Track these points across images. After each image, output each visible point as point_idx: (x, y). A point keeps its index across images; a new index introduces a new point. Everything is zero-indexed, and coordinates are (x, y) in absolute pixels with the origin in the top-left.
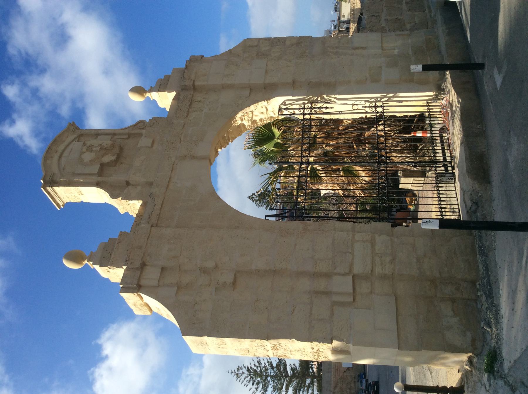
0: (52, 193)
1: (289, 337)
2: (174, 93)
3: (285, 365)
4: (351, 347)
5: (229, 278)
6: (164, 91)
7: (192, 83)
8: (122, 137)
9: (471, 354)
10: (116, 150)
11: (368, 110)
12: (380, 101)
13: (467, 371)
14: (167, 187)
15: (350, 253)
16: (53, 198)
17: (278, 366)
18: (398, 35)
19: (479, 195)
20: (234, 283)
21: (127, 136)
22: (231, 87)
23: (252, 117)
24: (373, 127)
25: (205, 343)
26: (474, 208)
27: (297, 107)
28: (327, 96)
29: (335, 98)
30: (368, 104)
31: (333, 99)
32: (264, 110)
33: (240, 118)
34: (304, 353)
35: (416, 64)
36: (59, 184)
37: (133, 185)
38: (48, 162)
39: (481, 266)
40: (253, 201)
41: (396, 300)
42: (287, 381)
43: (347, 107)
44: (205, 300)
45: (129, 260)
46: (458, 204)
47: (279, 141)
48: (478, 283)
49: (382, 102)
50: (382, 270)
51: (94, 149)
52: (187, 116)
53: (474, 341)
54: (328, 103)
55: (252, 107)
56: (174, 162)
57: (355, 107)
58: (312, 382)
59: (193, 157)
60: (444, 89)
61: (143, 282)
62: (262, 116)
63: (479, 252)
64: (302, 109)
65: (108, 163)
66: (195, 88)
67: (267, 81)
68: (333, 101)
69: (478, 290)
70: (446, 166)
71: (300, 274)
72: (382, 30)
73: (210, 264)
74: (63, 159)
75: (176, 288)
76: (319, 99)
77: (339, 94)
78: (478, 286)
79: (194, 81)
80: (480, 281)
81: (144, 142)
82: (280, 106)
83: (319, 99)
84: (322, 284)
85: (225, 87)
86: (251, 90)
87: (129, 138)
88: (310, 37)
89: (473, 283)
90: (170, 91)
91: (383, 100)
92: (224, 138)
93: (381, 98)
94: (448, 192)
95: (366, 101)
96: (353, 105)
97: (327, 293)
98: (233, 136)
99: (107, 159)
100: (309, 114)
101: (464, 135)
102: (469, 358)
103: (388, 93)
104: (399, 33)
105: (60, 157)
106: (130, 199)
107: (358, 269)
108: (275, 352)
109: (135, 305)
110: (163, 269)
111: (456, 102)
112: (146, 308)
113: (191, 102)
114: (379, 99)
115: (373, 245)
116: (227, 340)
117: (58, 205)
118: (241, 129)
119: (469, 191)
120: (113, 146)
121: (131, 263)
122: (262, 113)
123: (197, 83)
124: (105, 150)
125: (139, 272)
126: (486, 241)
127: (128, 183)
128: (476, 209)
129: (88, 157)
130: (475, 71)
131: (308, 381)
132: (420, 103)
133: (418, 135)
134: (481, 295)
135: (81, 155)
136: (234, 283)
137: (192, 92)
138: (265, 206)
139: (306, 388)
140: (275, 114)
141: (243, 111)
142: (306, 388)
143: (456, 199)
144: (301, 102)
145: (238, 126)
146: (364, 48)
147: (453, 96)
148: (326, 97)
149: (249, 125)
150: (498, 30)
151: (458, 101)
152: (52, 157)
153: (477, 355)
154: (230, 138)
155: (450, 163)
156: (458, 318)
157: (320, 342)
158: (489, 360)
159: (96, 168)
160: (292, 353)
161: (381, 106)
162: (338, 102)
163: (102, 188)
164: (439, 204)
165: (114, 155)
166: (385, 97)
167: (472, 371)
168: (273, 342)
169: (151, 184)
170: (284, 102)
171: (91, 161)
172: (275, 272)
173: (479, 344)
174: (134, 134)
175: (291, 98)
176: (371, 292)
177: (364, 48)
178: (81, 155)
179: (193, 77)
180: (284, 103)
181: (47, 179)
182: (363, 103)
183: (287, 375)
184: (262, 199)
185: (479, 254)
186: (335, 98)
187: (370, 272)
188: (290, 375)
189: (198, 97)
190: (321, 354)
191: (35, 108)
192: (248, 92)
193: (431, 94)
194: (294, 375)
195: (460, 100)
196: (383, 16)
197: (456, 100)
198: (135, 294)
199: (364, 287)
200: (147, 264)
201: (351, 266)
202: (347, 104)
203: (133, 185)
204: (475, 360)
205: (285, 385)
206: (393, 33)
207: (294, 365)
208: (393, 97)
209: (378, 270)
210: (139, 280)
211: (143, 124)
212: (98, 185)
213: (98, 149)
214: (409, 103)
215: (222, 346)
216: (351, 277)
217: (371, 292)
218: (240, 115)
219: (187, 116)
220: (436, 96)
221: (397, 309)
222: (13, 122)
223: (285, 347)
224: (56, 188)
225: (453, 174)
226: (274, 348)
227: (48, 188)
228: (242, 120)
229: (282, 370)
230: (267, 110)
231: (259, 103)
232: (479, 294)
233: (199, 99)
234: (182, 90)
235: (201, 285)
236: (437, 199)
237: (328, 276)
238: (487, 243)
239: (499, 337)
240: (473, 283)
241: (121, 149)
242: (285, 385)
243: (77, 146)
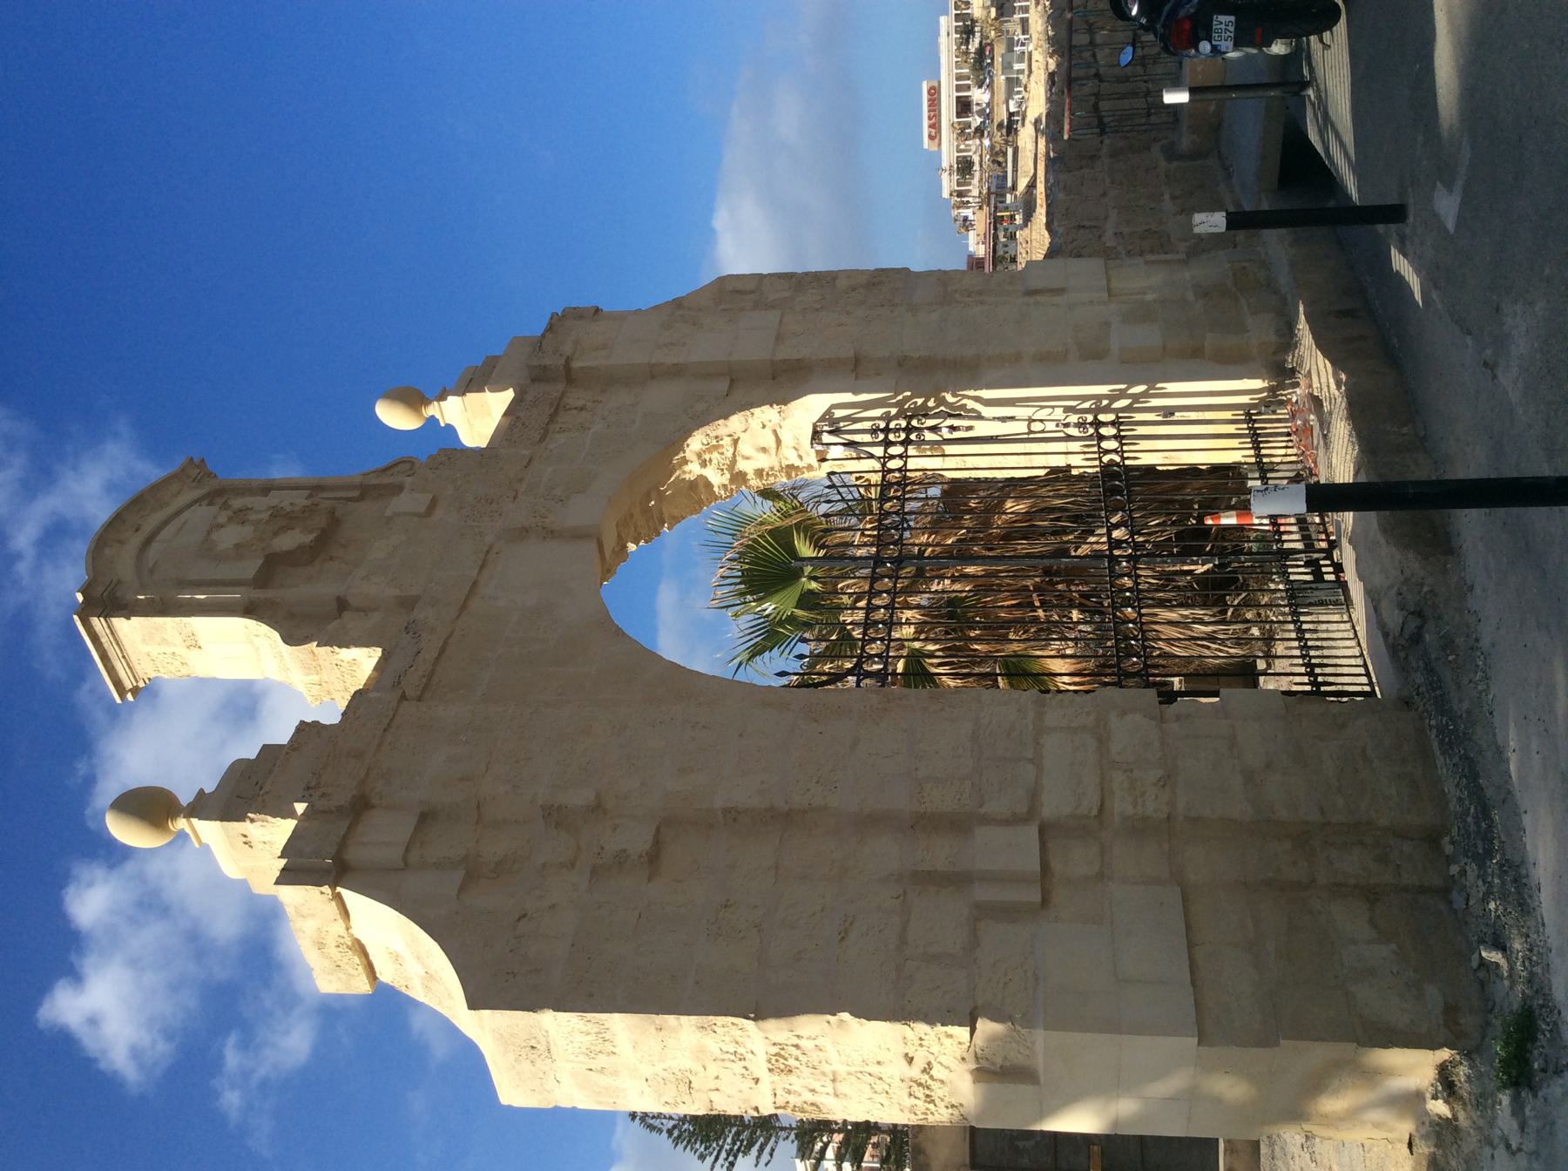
0: (104, 640)
1: (828, 1007)
2: (509, 395)
4: (1041, 1044)
5: (637, 840)
6: (481, 390)
7: (562, 361)
8: (343, 494)
9: (1445, 1054)
10: (321, 521)
11: (1074, 431)
12: (1107, 410)
13: (1442, 1131)
14: (464, 607)
15: (1031, 761)
16: (104, 657)
18: (1153, 262)
19: (1425, 589)
20: (653, 858)
21: (356, 494)
22: (677, 371)
23: (734, 461)
24: (1092, 533)
25: (541, 1047)
26: (1413, 625)
27: (867, 425)
28: (954, 395)
29: (977, 399)
30: (1074, 418)
31: (971, 404)
32: (770, 442)
33: (699, 455)
34: (879, 1086)
35: (1212, 208)
36: (128, 610)
37: (358, 610)
38: (108, 552)
39: (1450, 788)
41: (1185, 899)
43: (1016, 433)
44: (553, 907)
45: (318, 786)
46: (1362, 655)
47: (814, 585)
48: (1447, 839)
49: (1117, 411)
50: (1135, 805)
51: (253, 517)
52: (542, 439)
53: (1451, 1010)
54: (959, 416)
55: (736, 422)
56: (491, 547)
57: (1036, 426)
59: (551, 534)
60: (1293, 371)
61: (353, 854)
62: (764, 462)
63: (1441, 743)
64: (882, 431)
65: (289, 553)
66: (569, 376)
67: (780, 356)
68: (973, 410)
69: (1450, 860)
70: (1314, 565)
71: (868, 823)
72: (1108, 254)
74: (155, 546)
75: (458, 875)
76: (931, 403)
77: (989, 386)
78: (1448, 849)
79: (568, 360)
80: (1454, 831)
81: (406, 502)
82: (815, 426)
83: (931, 403)
84: (940, 853)
85: (653, 374)
86: (732, 380)
87: (361, 498)
88: (905, 272)
89: (1432, 838)
90: (499, 387)
91: (1117, 405)
92: (646, 510)
93: (1113, 398)
94: (1324, 627)
95: (1068, 410)
96: (1031, 421)
97: (959, 880)
98: (676, 512)
99: (288, 541)
100: (902, 443)
101: (1361, 451)
102: (1444, 1071)
103: (1132, 384)
104: (1153, 258)
105: (148, 542)
106: (344, 644)
107: (1054, 804)
108: (782, 1081)
109: (321, 946)
110: (426, 818)
111: (1333, 386)
112: (357, 960)
113: (558, 408)
114: (1105, 402)
115: (1102, 737)
116: (618, 1023)
117: (118, 684)
118: (698, 491)
119: (1389, 588)
120: (309, 511)
121: (323, 795)
122: (764, 450)
123: (576, 364)
124: (283, 519)
125: (343, 825)
126: (1461, 701)
127: (342, 605)
128: (1420, 628)
129: (229, 537)
130: (1375, 479)
132: (1228, 415)
133: (1224, 521)
134: (1463, 873)
135: (209, 533)
136: (653, 858)
137: (561, 387)
140: (800, 457)
141: (707, 429)
143: (1353, 643)
144: (878, 412)
145: (691, 482)
146: (1060, 291)
147: (1323, 373)
148: (950, 398)
149: (724, 486)
150: (1434, 95)
151: (1338, 384)
152: (121, 542)
153: (1468, 1054)
154: (666, 516)
155: (1329, 556)
156: (1394, 946)
157: (931, 1023)
158: (1510, 1050)
159: (249, 568)
160: (842, 1088)
161: (1113, 423)
162: (987, 411)
163: (260, 619)
164: (1303, 657)
165: (311, 532)
166: (1122, 395)
167: (1455, 1118)
168: (777, 1030)
169: (408, 603)
170: (829, 412)
171: (237, 546)
172: (787, 819)
173: (1469, 1022)
174: (375, 487)
175: (848, 397)
176: (1101, 876)
177: (1060, 291)
178: (209, 533)
179: (567, 349)
180: (827, 417)
181: (98, 591)
182: (1059, 414)
185: (1443, 754)
186: (977, 399)
187: (1095, 812)
189: (576, 397)
190: (938, 1091)
191: (150, 935)
192: (723, 386)
193: (1257, 384)
195: (1343, 377)
196: (1110, 229)
197: (1332, 380)
198: (326, 889)
199: (1076, 860)
200: (374, 801)
201: (1034, 795)
202: (1012, 418)
203: (358, 610)
204: (1462, 1072)
206: (1140, 260)
208: (1145, 394)
209: (1121, 805)
210: (343, 844)
211: (408, 466)
214: (1192, 423)
215: (602, 1061)
216: (1033, 831)
217: (1101, 876)
218: (696, 442)
219: (542, 439)
220: (1272, 390)
221: (1188, 927)
222: (77, 977)
223: (814, 1057)
224: (119, 623)
225: (1343, 585)
226: (780, 1064)
227: (95, 621)
228: (704, 464)
230: (778, 442)
231: (756, 411)
232: (1454, 869)
233: (580, 403)
234: (533, 381)
235: (544, 865)
236: (1296, 644)
237: (958, 824)
238: (1465, 706)
239: (1537, 955)
240: (1432, 838)
241: (335, 522)
243: (202, 514)
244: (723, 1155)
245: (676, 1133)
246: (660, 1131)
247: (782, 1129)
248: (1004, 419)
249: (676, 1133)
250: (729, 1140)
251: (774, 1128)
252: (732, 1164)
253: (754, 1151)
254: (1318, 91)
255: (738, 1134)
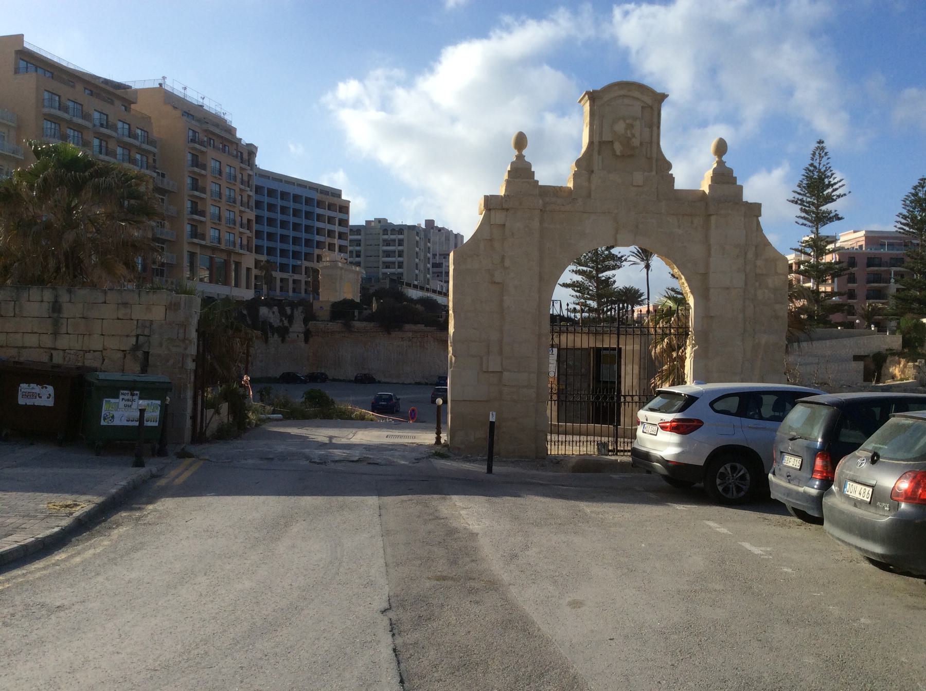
3: (614, 268)
5: (498, 277)
17: (613, 257)
20: (494, 283)
36: (591, 106)
40: (915, 188)
42: (591, 272)
58: (591, 310)
59: (617, 231)
61: (493, 212)
73: (507, 263)
107: (506, 375)
129: (620, 127)
131: (594, 304)
136: (494, 283)
138: (905, 212)
139: (582, 300)
142: (582, 300)
159: (607, 137)
169: (589, 195)
183: (599, 271)
184: (921, 205)
188: (600, 275)
194: (598, 280)
205: (585, 269)
207: (615, 282)
212: (591, 143)
213: (629, 135)
229: (606, 263)
237: (501, 353)
242: (585, 269)
244: (800, 197)
245: (812, 168)
246: (812, 159)
247: (817, 229)
248: (401, 437)
249: (812, 168)
250: (809, 199)
251: (817, 224)
252: (796, 203)
253: (803, 215)
254: (219, 149)
255: (813, 204)
